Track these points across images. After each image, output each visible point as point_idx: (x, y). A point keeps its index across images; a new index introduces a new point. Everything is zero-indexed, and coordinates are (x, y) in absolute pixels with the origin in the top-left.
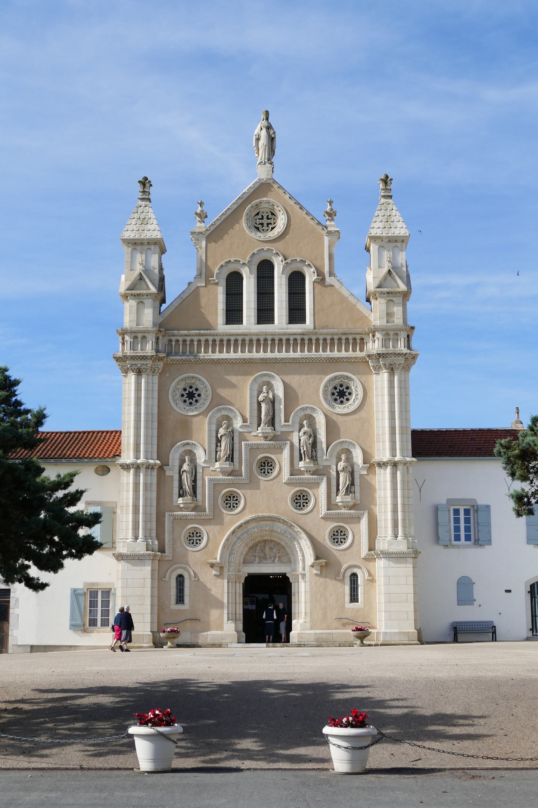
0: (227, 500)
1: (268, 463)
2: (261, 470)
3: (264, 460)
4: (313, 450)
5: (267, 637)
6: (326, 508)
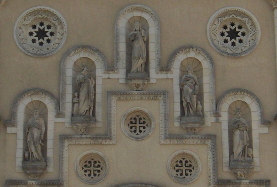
0: (86, 166)
1: (140, 119)
2: (131, 128)
3: (134, 116)
4: (199, 102)
5: (264, 163)
6: (55, 114)
